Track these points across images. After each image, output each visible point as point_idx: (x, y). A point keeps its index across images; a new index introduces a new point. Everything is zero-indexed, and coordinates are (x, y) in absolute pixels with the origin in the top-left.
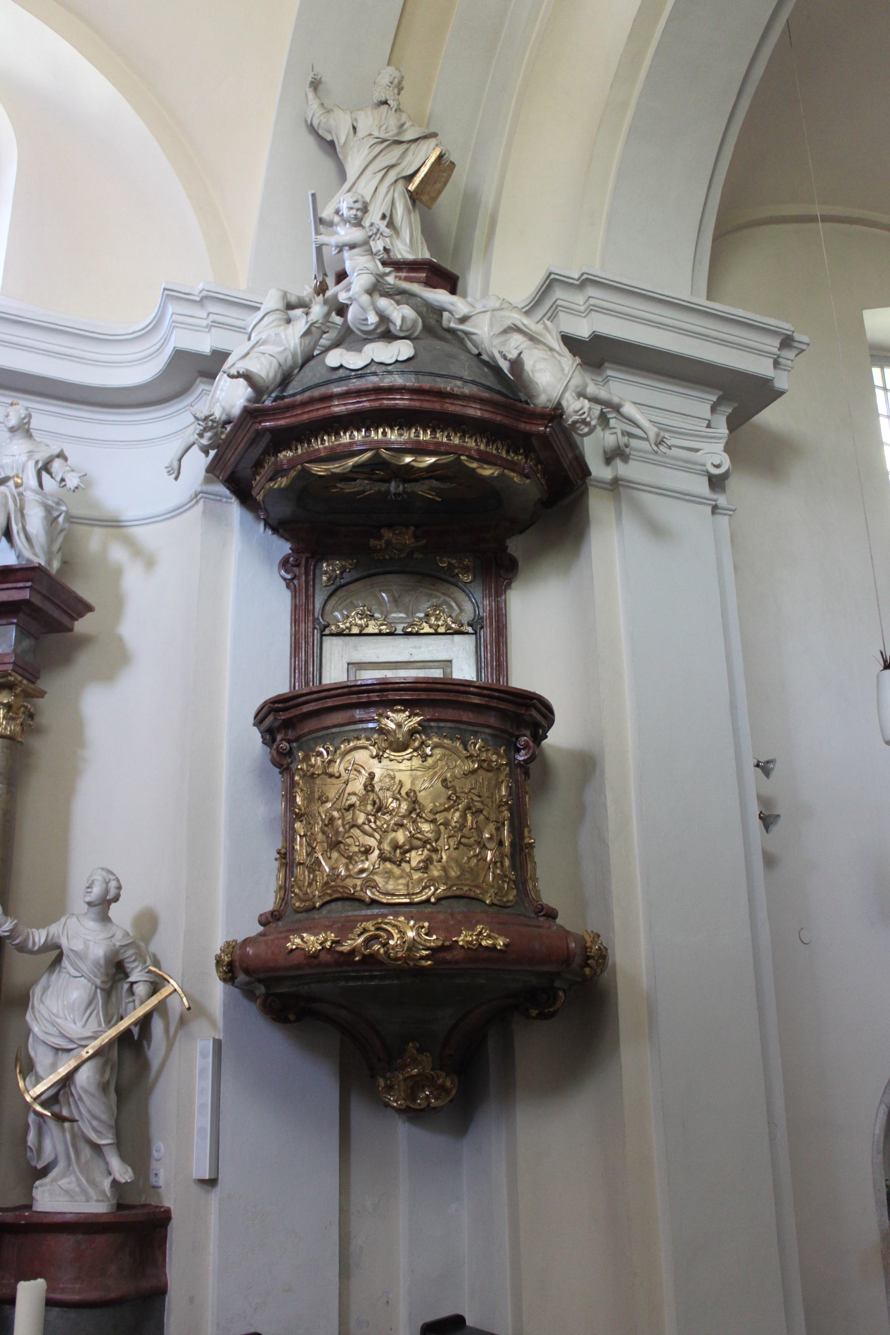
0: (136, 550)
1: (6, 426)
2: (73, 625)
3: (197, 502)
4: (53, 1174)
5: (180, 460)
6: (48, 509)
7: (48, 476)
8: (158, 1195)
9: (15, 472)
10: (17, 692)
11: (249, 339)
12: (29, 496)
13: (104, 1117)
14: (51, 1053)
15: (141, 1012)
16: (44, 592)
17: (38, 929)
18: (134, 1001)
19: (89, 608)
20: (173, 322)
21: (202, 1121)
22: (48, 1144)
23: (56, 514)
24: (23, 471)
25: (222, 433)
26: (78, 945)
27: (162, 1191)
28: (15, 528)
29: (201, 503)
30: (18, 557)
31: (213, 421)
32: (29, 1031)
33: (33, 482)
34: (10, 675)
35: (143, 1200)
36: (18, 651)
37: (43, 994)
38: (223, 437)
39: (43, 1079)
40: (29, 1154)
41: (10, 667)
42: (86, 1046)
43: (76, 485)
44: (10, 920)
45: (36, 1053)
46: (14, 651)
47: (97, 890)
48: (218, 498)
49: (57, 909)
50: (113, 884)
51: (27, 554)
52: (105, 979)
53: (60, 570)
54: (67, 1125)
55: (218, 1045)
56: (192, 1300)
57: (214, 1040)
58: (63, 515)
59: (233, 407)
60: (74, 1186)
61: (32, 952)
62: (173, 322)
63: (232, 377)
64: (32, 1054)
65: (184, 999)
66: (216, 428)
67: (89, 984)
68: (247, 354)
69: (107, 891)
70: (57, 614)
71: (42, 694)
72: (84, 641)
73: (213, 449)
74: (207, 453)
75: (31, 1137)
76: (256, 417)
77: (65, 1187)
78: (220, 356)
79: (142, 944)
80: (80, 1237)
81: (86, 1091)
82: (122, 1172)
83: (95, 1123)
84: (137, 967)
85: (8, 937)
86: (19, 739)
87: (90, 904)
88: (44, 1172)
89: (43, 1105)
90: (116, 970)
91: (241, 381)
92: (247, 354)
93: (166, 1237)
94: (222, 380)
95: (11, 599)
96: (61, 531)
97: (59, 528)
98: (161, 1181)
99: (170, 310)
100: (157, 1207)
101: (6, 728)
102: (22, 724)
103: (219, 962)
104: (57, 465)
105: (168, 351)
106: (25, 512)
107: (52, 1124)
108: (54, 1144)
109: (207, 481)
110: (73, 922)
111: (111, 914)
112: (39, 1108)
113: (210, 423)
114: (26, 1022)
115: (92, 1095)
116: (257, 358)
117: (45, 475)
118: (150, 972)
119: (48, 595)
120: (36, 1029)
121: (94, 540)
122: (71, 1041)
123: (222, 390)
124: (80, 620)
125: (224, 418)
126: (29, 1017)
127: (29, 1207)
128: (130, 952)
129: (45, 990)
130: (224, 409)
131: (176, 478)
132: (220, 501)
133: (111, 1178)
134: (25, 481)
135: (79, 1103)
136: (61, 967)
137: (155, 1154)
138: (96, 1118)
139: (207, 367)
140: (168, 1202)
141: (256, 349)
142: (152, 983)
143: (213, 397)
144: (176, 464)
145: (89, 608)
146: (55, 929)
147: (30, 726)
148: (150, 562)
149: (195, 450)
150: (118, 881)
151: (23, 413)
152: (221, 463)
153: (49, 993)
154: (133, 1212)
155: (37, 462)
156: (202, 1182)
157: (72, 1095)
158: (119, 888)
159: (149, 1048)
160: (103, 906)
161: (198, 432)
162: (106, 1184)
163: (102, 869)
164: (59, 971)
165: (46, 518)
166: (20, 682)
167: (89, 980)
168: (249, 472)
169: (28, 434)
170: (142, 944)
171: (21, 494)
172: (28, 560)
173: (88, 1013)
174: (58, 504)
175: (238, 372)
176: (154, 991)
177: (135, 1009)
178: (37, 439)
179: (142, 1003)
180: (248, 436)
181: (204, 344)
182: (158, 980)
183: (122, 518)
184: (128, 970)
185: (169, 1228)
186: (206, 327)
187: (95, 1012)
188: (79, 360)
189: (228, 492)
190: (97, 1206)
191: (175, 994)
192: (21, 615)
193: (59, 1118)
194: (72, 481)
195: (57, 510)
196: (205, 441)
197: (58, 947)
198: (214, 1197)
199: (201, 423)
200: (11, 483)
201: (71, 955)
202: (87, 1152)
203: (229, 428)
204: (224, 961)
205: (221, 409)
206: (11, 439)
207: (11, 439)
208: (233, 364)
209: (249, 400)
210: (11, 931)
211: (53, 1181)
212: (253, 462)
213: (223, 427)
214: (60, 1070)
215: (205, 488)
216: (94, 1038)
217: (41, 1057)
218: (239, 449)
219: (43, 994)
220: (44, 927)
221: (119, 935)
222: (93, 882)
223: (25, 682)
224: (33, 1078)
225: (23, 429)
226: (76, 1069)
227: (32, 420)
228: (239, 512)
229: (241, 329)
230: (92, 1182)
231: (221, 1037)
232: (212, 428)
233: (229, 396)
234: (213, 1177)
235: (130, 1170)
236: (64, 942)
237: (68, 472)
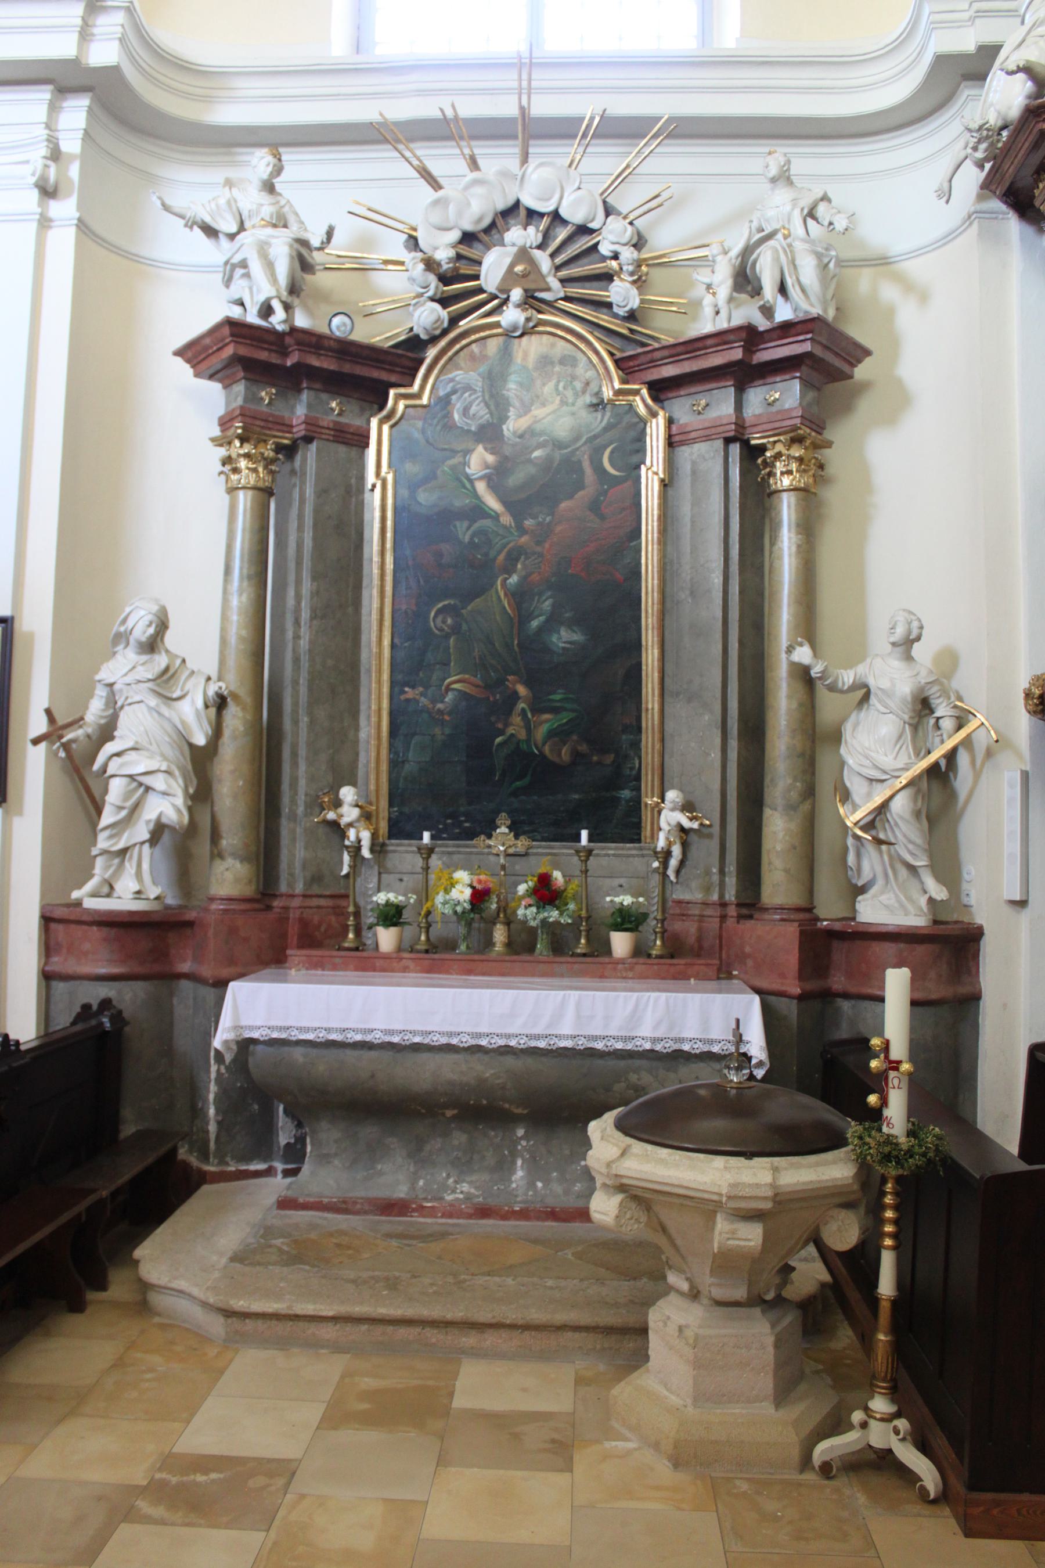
0: (908, 286)
1: (766, 177)
2: (853, 372)
3: (971, 224)
4: (872, 891)
5: (950, 181)
6: (819, 256)
7: (814, 222)
8: (970, 914)
9: (781, 223)
10: (807, 444)
11: (1023, 23)
12: (798, 246)
13: (919, 841)
14: (866, 783)
15: (949, 745)
16: (824, 342)
17: (846, 669)
18: (942, 735)
19: (867, 353)
20: (932, 23)
21: (1012, 847)
22: (866, 865)
23: (826, 260)
24: (789, 221)
25: (998, 141)
26: (885, 684)
27: (973, 910)
28: (789, 282)
29: (975, 225)
30: (795, 310)
31: (988, 130)
32: (842, 763)
33: (800, 231)
34: (800, 428)
35: (955, 917)
36: (804, 404)
37: (854, 730)
38: (1000, 145)
39: (860, 807)
40: (850, 873)
41: (798, 421)
42: (899, 777)
43: (845, 227)
44: (820, 662)
45: (852, 784)
46: (800, 404)
47: (900, 632)
48: (994, 216)
49: (858, 653)
50: (915, 624)
51: (804, 306)
52: (913, 714)
53: (835, 318)
54: (884, 847)
55: (1025, 776)
56: (1005, 1006)
57: (1022, 772)
58: (833, 261)
59: (1010, 108)
60: (893, 902)
61: (842, 692)
62: (932, 23)
63: (1011, 73)
64: (848, 784)
65: (992, 732)
66: (992, 136)
67: (898, 720)
68: (1023, 41)
69: (910, 632)
70: (837, 363)
71: (829, 444)
72: (864, 387)
73: (989, 162)
74: (981, 167)
75: (851, 859)
76: (1039, 115)
77: (886, 902)
78: (989, 52)
79: (945, 681)
80: (902, 945)
81: (901, 818)
82: (940, 893)
83: (911, 847)
84: (941, 703)
85: (820, 678)
86: (813, 490)
87: (894, 644)
88: (862, 890)
89: (862, 829)
90: (923, 706)
91: (1021, 76)
92: (1023, 41)
93: (979, 950)
94: (997, 79)
95: (793, 353)
96: (834, 277)
97: (831, 275)
98: (973, 901)
99: (926, 10)
100: (970, 924)
101: (800, 481)
102: (814, 476)
103: (1028, 695)
104: (822, 210)
105: (928, 59)
106: (797, 262)
107: (870, 849)
108: (870, 864)
109: (980, 198)
110: (878, 662)
111: (914, 653)
112: (860, 833)
113: (985, 133)
114: (840, 756)
115: (908, 821)
116: (1036, 43)
117: (810, 221)
118: (955, 707)
119: (829, 345)
120: (850, 761)
121: (864, 281)
122: (885, 772)
123: (996, 91)
124: (860, 366)
125: (1000, 123)
126: (843, 751)
127: (854, 919)
128: (935, 688)
129: (856, 725)
130: (999, 113)
131: (947, 202)
132: (996, 218)
133: (927, 896)
134: (792, 231)
135: (895, 829)
136: (869, 705)
137: (966, 876)
138: (911, 842)
139: (975, 67)
140: (979, 920)
141: (1032, 34)
142: (957, 718)
143: (985, 101)
144: (946, 185)
145: (867, 353)
146: (861, 669)
147: (822, 476)
148: (923, 296)
149: (968, 165)
150: (920, 621)
151: (782, 160)
152: (998, 175)
153: (860, 728)
154: (950, 927)
155: (802, 209)
156: (1013, 903)
157: (888, 821)
158: (921, 628)
159: (955, 778)
160: (907, 644)
161: (971, 145)
162: (923, 901)
163: (904, 610)
164: (868, 709)
165: (818, 266)
166: (809, 434)
167: (897, 716)
168: (1030, 180)
169: (789, 182)
170: (945, 681)
171: (790, 246)
172: (806, 312)
173: (898, 746)
174: (827, 249)
175: (1018, 66)
176: (959, 727)
177: (942, 742)
178: (799, 185)
179: (950, 737)
180: (1030, 139)
181: (966, 42)
182: (962, 715)
183: (890, 255)
184: (934, 706)
185: (982, 943)
186: (969, 20)
187: (904, 747)
188: (830, 90)
189: (1003, 207)
190: (916, 919)
191: (982, 729)
192: (804, 368)
193: (879, 842)
194: (840, 224)
195: (827, 256)
196: (980, 155)
197: (866, 686)
198: (1025, 917)
199: (975, 134)
200: (779, 236)
201: (879, 693)
202: (903, 872)
203: (1005, 133)
204: (1034, 694)
205: (996, 114)
206: (773, 189)
207: (773, 189)
208: (1010, 57)
209: (1029, 97)
210: (823, 672)
211: (874, 896)
212: (1034, 168)
213: (999, 134)
214: (877, 799)
215: (979, 207)
216: (906, 769)
217: (856, 787)
218: (1020, 155)
219: (854, 730)
220: (851, 668)
221: (924, 673)
222: (896, 623)
223: (813, 434)
224: (850, 806)
225: (784, 178)
226: (892, 797)
227: (792, 167)
228: (1018, 227)
229: (1011, 13)
230: (910, 899)
231: (1028, 769)
232: (987, 137)
233: (1006, 96)
234: (1024, 898)
235: (944, 889)
236: (872, 682)
237: (836, 214)
